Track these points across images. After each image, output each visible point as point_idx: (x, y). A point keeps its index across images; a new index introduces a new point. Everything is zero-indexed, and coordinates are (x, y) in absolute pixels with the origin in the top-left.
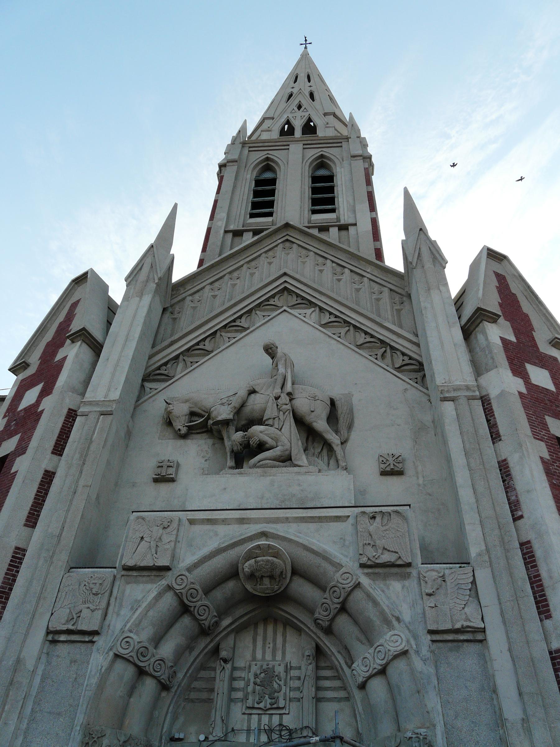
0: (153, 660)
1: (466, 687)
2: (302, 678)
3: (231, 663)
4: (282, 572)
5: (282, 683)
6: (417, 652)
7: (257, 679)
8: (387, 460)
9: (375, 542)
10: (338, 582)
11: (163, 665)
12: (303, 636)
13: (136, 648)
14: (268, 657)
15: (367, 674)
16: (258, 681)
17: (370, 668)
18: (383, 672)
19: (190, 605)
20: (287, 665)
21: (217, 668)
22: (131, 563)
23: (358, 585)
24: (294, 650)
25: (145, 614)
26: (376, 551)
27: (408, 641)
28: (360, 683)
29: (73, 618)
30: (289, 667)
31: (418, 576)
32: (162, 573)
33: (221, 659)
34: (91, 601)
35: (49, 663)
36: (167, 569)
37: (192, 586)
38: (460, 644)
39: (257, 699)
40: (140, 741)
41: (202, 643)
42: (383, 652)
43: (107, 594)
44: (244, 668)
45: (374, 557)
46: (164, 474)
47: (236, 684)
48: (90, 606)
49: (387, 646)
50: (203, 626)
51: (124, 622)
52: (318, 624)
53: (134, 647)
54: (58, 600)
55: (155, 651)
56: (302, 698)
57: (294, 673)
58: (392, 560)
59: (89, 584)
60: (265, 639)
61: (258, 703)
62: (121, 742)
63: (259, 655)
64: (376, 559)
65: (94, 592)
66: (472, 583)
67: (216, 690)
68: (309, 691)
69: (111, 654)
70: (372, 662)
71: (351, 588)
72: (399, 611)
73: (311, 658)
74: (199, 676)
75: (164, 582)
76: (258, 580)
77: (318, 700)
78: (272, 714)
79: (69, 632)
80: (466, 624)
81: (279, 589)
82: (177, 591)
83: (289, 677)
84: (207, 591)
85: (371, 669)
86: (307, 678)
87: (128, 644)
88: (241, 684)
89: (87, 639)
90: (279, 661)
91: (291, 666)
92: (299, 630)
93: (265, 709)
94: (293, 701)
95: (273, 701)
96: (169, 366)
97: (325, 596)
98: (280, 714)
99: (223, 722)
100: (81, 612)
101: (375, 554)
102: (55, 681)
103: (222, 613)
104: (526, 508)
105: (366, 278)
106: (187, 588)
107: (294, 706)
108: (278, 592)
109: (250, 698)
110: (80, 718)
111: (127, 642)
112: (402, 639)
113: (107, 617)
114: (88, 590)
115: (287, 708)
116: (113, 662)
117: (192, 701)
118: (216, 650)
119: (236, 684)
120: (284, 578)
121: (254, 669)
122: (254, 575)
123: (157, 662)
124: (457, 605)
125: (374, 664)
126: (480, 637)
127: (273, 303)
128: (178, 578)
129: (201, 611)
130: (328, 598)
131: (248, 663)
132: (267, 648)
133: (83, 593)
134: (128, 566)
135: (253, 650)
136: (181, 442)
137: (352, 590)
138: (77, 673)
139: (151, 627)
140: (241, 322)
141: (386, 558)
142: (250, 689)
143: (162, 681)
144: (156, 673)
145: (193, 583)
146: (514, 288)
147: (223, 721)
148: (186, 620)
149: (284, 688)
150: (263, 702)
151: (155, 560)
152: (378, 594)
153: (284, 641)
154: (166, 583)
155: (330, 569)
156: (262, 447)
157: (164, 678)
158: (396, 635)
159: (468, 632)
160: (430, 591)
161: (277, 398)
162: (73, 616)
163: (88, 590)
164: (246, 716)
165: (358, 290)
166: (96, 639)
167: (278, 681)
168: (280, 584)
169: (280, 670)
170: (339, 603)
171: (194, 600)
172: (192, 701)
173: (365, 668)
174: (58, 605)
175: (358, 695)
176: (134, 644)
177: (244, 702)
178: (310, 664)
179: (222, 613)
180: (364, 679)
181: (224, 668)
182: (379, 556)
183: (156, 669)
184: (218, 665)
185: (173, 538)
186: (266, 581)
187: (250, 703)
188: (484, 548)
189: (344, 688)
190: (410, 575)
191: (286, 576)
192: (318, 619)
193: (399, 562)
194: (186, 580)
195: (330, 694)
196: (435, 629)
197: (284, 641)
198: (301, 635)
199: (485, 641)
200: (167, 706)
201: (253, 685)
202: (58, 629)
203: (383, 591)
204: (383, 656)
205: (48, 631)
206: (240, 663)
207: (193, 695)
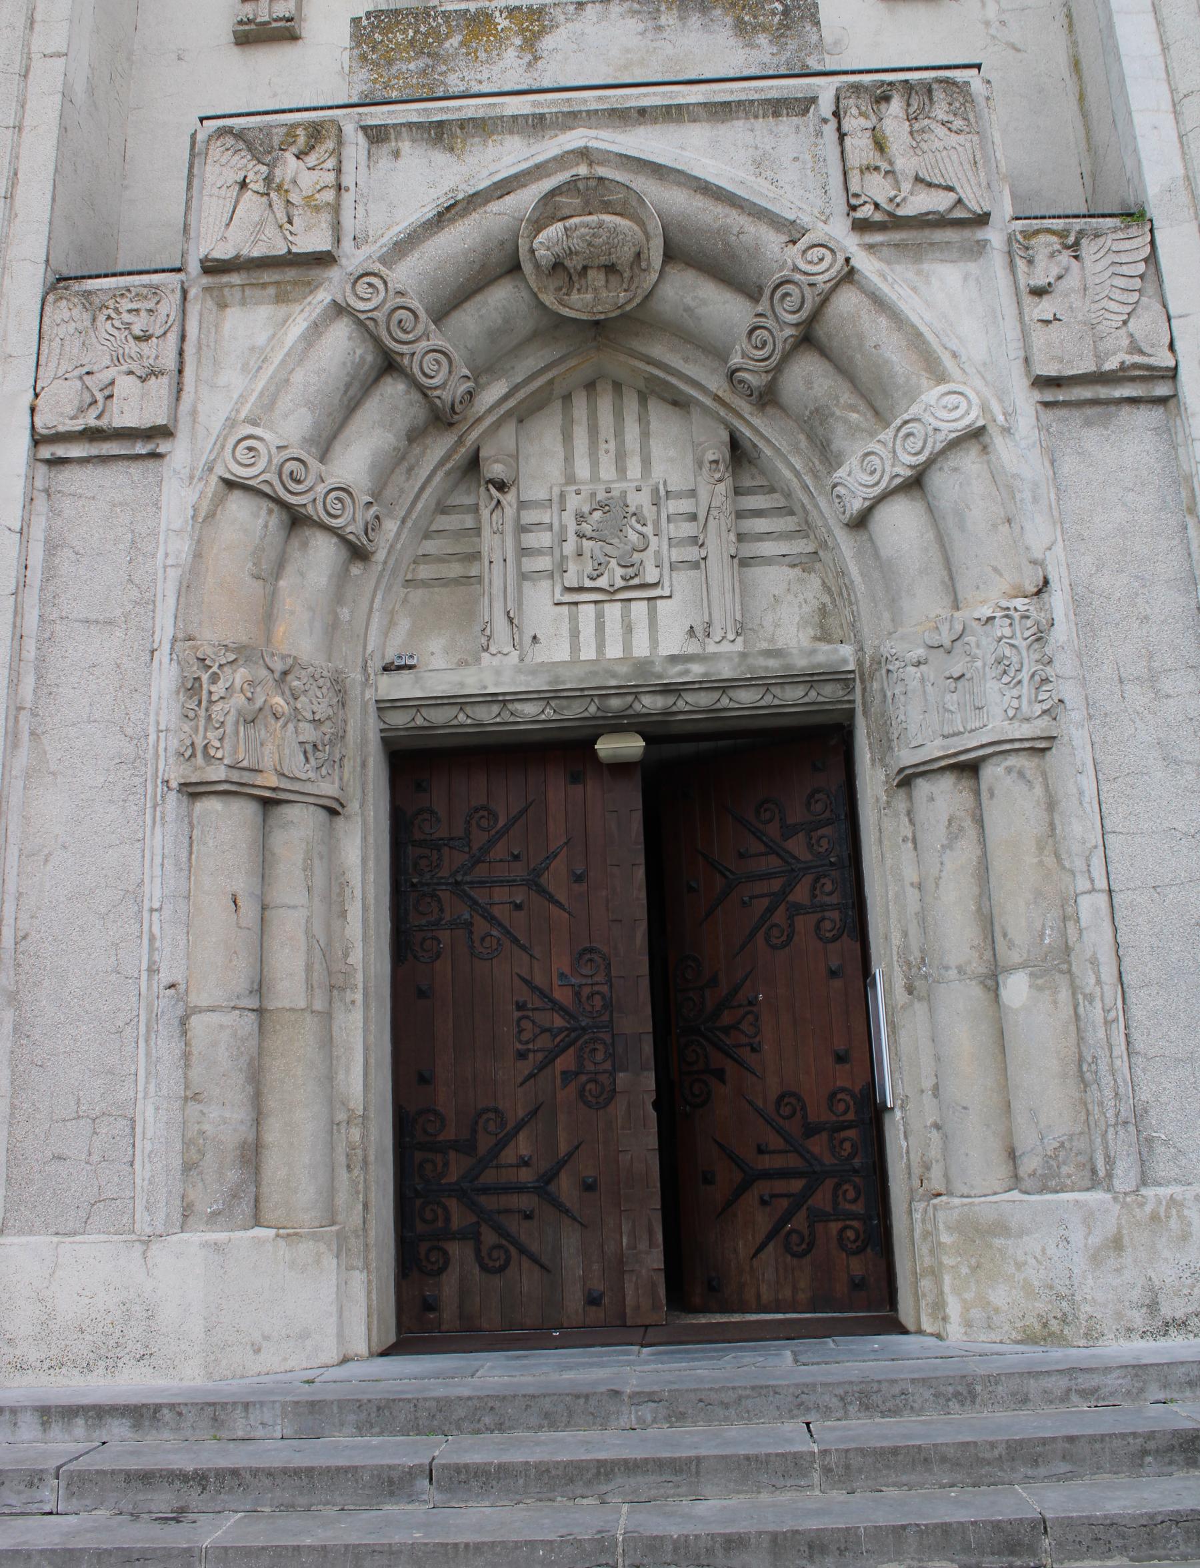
0: (321, 489)
1: (1124, 505)
2: (702, 517)
3: (513, 490)
4: (639, 254)
5: (648, 530)
6: (1007, 431)
7: (584, 524)
9: (891, 163)
10: (796, 269)
11: (348, 500)
12: (696, 413)
13: (275, 461)
14: (607, 471)
15: (877, 491)
16: (587, 528)
17: (882, 476)
18: (915, 483)
19: (400, 351)
20: (657, 490)
21: (482, 504)
22: (223, 252)
23: (849, 275)
24: (672, 453)
25: (281, 383)
27: (985, 408)
28: (855, 512)
29: (96, 402)
30: (662, 493)
31: (1006, 249)
32: (315, 273)
33: (491, 481)
34: (133, 355)
35: (55, 512)
36: (324, 260)
37: (400, 301)
38: (1113, 408)
39: (589, 569)
40: (319, 670)
41: (438, 448)
42: (920, 433)
43: (173, 337)
44: (547, 503)
45: (891, 200)
46: (266, 19)
47: (530, 540)
48: (134, 366)
49: (931, 420)
50: (438, 401)
51: (233, 402)
52: (740, 382)
53: (270, 461)
54: (42, 361)
55: (323, 468)
56: (704, 559)
57: (673, 506)
58: (942, 208)
59: (119, 313)
60: (593, 430)
62: (277, 675)
63: (582, 469)
64: (898, 205)
65: (138, 333)
66: (1146, 260)
67: (485, 554)
68: (719, 544)
69: (214, 480)
70: (888, 463)
71: (832, 283)
72: (958, 337)
73: (722, 467)
74: (434, 527)
75: (323, 297)
76: (575, 278)
78: (630, 600)
79: (93, 435)
81: (630, 301)
82: (362, 317)
83: (664, 516)
84: (440, 315)
85: (886, 478)
86: (714, 512)
87: (252, 454)
88: (544, 539)
89: (141, 448)
90: (636, 480)
91: (667, 492)
92: (680, 403)
93: (611, 589)
94: (678, 569)
95: (631, 571)
97: (760, 309)
98: (649, 599)
99: (512, 623)
100: (112, 383)
101: (893, 193)
102: (82, 551)
103: (482, 372)
106: (388, 306)
107: (682, 581)
108: (628, 308)
109: (572, 567)
110: (165, 628)
111: (250, 449)
112: (969, 401)
113: (184, 395)
114: (118, 329)
115: (667, 584)
116: (218, 502)
117: (425, 584)
118: (473, 464)
119: (530, 540)
120: (644, 270)
121: (574, 503)
122: (562, 264)
123: (333, 494)
124: (1108, 315)
125: (893, 466)
126: (1162, 390)
128: (360, 281)
129: (429, 364)
130: (769, 313)
131: (556, 491)
132: (601, 453)
133: (108, 337)
134: (217, 260)
135: (566, 459)
137: (834, 289)
138: (133, 531)
139: (304, 410)
142: (569, 548)
143: (351, 537)
144: (424, 379)
145: (400, 293)
147: (511, 620)
148: (394, 389)
149: (654, 541)
150: (606, 575)
151: (290, 238)
153: (645, 434)
154: (329, 299)
155: (772, 241)
157: (354, 530)
158: (955, 393)
159: (1133, 379)
160: (1040, 281)
162: (93, 395)
163: (118, 329)
164: (565, 609)
167: (638, 527)
168: (633, 287)
169: (640, 500)
170: (797, 325)
171: (410, 337)
172: (425, 584)
173: (869, 478)
174: (46, 374)
175: (846, 543)
176: (269, 452)
177: (556, 576)
178: (720, 480)
179: (482, 372)
180: (867, 504)
181: (499, 502)
182: (904, 199)
183: (333, 512)
184: (484, 498)
185: (330, 178)
186: (596, 278)
187: (571, 580)
188: (1180, 171)
189: (805, 530)
190: (984, 247)
191: (649, 264)
192: (737, 370)
193: (959, 214)
194: (381, 287)
195: (768, 548)
196: (1053, 374)
197: (645, 434)
198: (688, 413)
199: (1174, 400)
200: (368, 595)
201: (575, 538)
202: (61, 429)
203: (914, 289)
204: (920, 444)
205: (37, 437)
206: (534, 490)
207: (425, 572)
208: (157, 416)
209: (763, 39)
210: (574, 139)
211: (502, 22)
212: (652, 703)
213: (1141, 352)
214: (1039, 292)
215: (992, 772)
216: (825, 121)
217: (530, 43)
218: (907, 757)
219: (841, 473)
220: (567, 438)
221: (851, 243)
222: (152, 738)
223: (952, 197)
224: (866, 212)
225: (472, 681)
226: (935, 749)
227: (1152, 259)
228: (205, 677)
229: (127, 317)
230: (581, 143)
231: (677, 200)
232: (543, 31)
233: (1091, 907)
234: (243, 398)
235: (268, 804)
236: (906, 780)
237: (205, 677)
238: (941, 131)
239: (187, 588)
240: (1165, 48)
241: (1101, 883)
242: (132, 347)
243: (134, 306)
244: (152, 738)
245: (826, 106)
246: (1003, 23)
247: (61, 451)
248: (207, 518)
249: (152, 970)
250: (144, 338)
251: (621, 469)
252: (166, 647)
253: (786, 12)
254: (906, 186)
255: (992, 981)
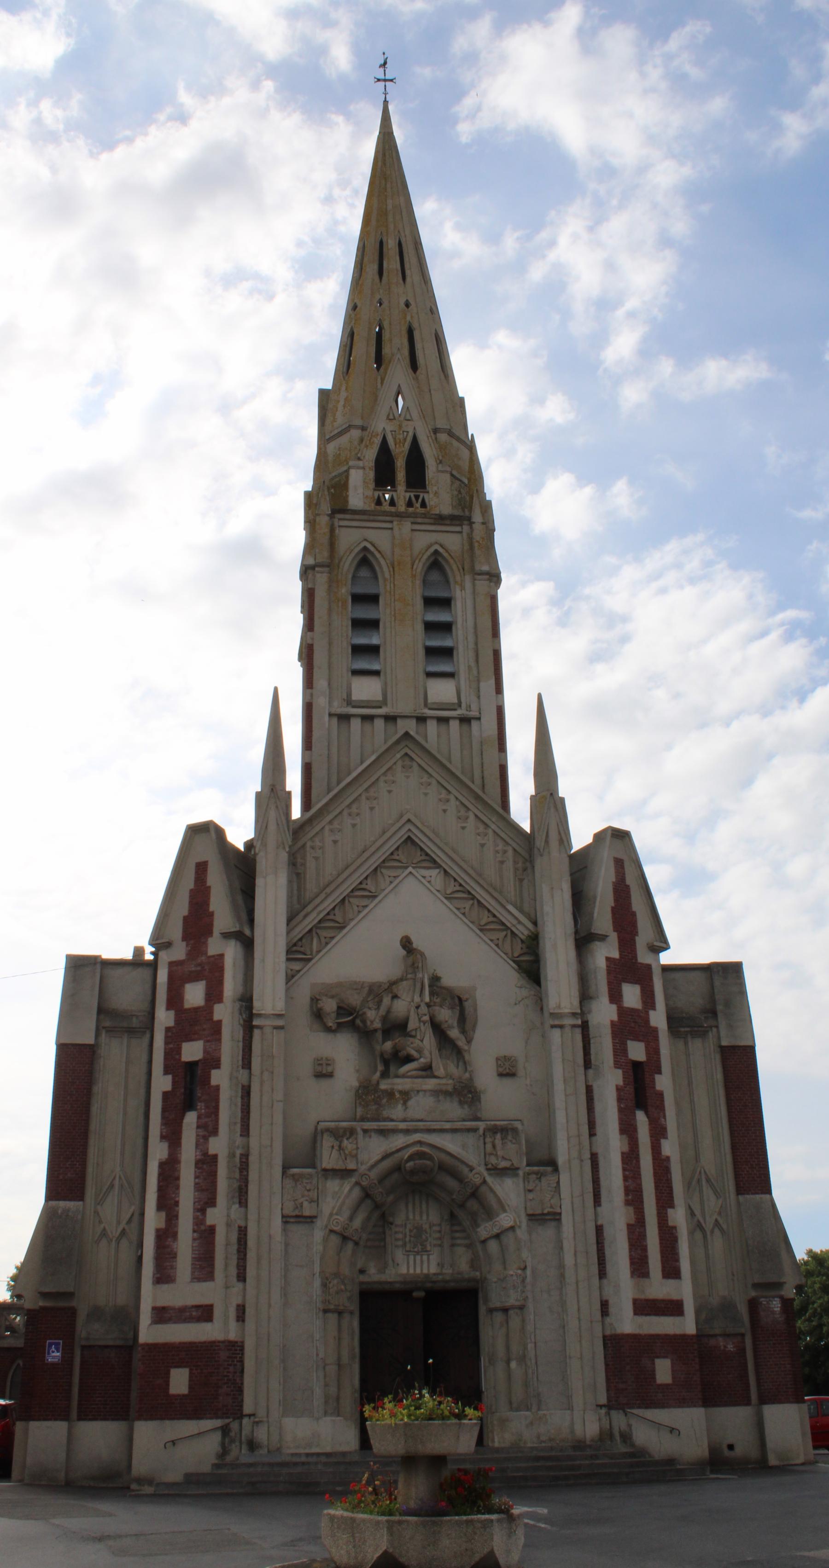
5: (428, 1235)
6: (520, 1227)
8: (504, 1064)
9: (497, 1152)
14: (418, 1217)
18: (497, 1236)
22: (329, 1167)
25: (343, 1203)
26: (498, 1160)
27: (515, 1221)
60: (414, 1204)
61: (414, 1248)
63: (411, 1217)
75: (353, 1180)
77: (453, 1245)
79: (297, 1216)
80: (551, 1210)
88: (400, 1236)
96: (304, 941)
104: (599, 1130)
105: (490, 830)
110: (317, 1269)
121: (409, 1226)
127: (397, 858)
136: (330, 1036)
140: (367, 884)
141: (503, 1164)
142: (407, 1239)
146: (630, 880)
152: (498, 1189)
155: (466, 1170)
156: (409, 1059)
160: (531, 1188)
161: (418, 1007)
165: (482, 845)
166: (314, 1220)
169: (426, 1226)
175: (479, 1247)
187: (408, 1248)
195: (459, 1242)
208: (314, 1213)
209: (466, 1106)
210: (417, 1137)
211: (397, 1095)
212: (429, 1285)
213: (553, 1208)
214: (530, 1191)
215: (511, 1312)
216: (481, 1136)
217: (405, 1103)
218: (492, 1305)
219: (479, 1230)
220: (407, 1207)
221: (485, 1174)
222: (315, 1297)
223: (510, 1163)
224: (490, 1166)
225: (383, 1278)
226: (498, 1305)
227: (558, 1183)
228: (328, 1282)
229: (305, 1185)
230: (419, 1139)
231: (443, 1156)
232: (409, 1099)
233: (530, 1346)
234: (334, 1208)
235: (340, 1313)
236: (491, 1311)
237: (328, 1282)
238: (509, 1143)
239: (322, 1258)
240: (567, 1122)
241: (533, 1340)
242: (306, 1193)
243: (307, 1181)
244: (315, 1297)
245: (481, 1131)
246: (531, 1085)
247: (288, 1219)
248: (325, 1240)
249: (317, 1355)
250: (309, 1190)
251: (421, 1216)
252: (318, 1274)
253: (472, 1098)
254: (500, 1159)
255: (508, 1362)
